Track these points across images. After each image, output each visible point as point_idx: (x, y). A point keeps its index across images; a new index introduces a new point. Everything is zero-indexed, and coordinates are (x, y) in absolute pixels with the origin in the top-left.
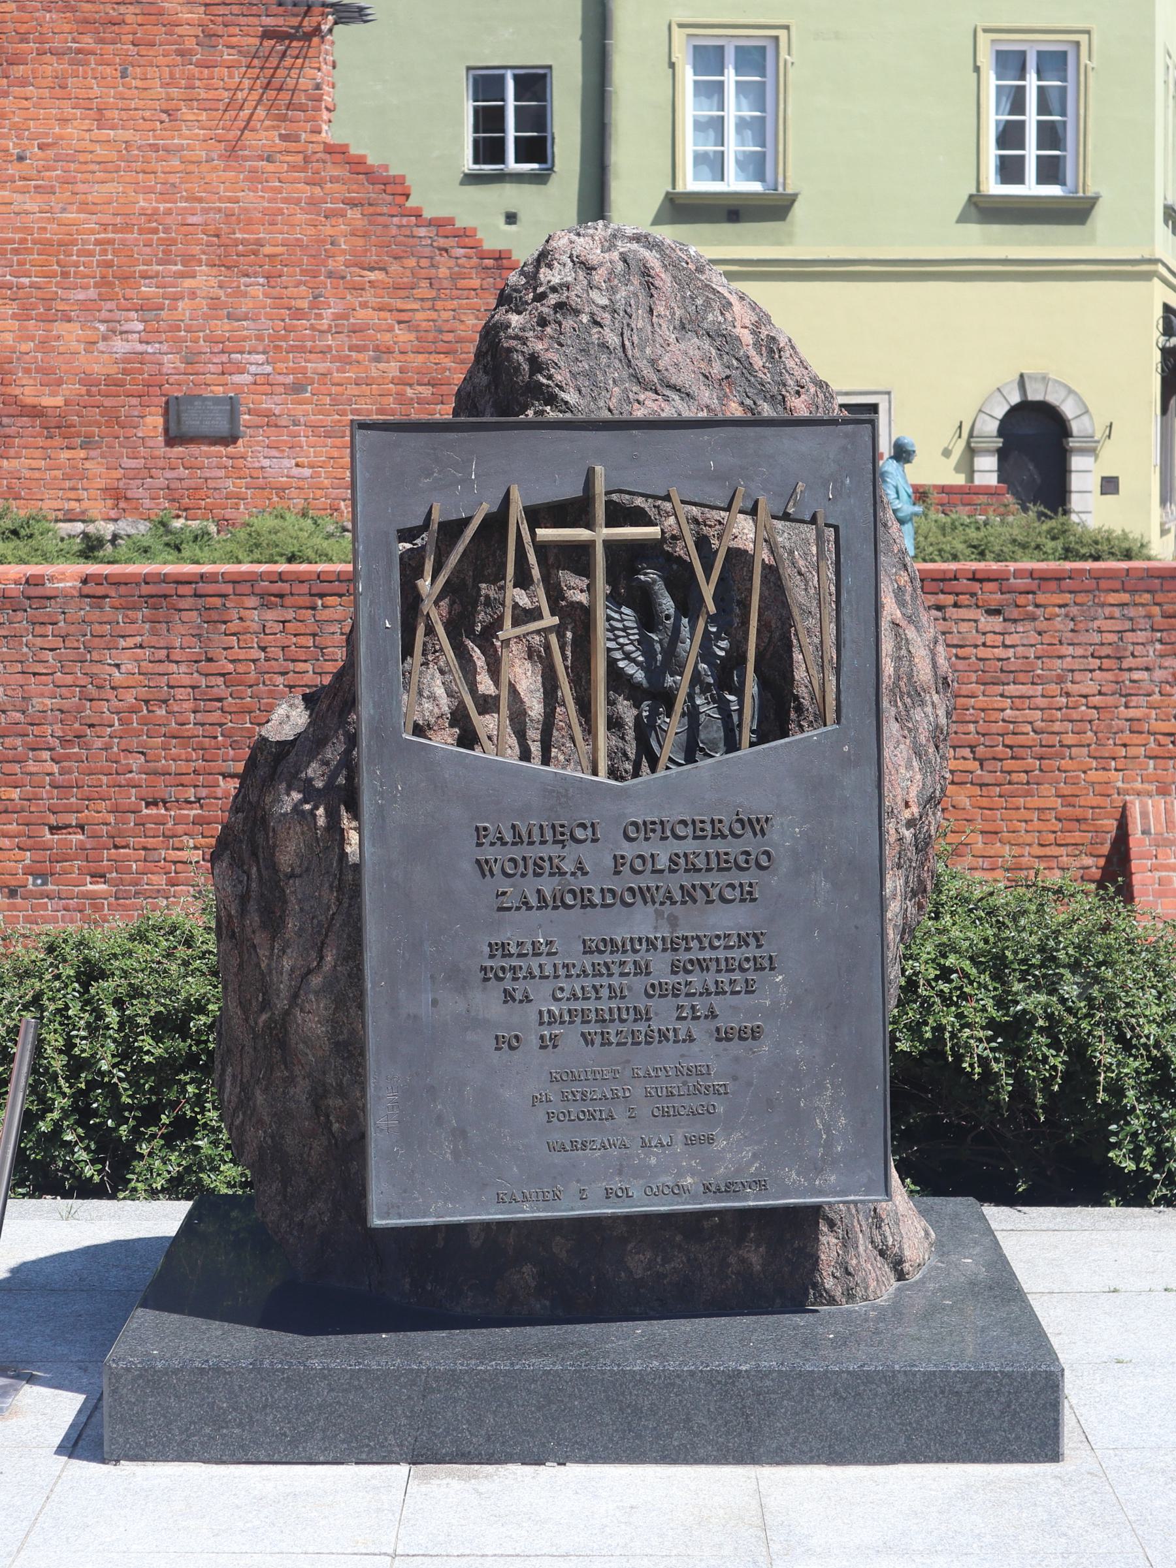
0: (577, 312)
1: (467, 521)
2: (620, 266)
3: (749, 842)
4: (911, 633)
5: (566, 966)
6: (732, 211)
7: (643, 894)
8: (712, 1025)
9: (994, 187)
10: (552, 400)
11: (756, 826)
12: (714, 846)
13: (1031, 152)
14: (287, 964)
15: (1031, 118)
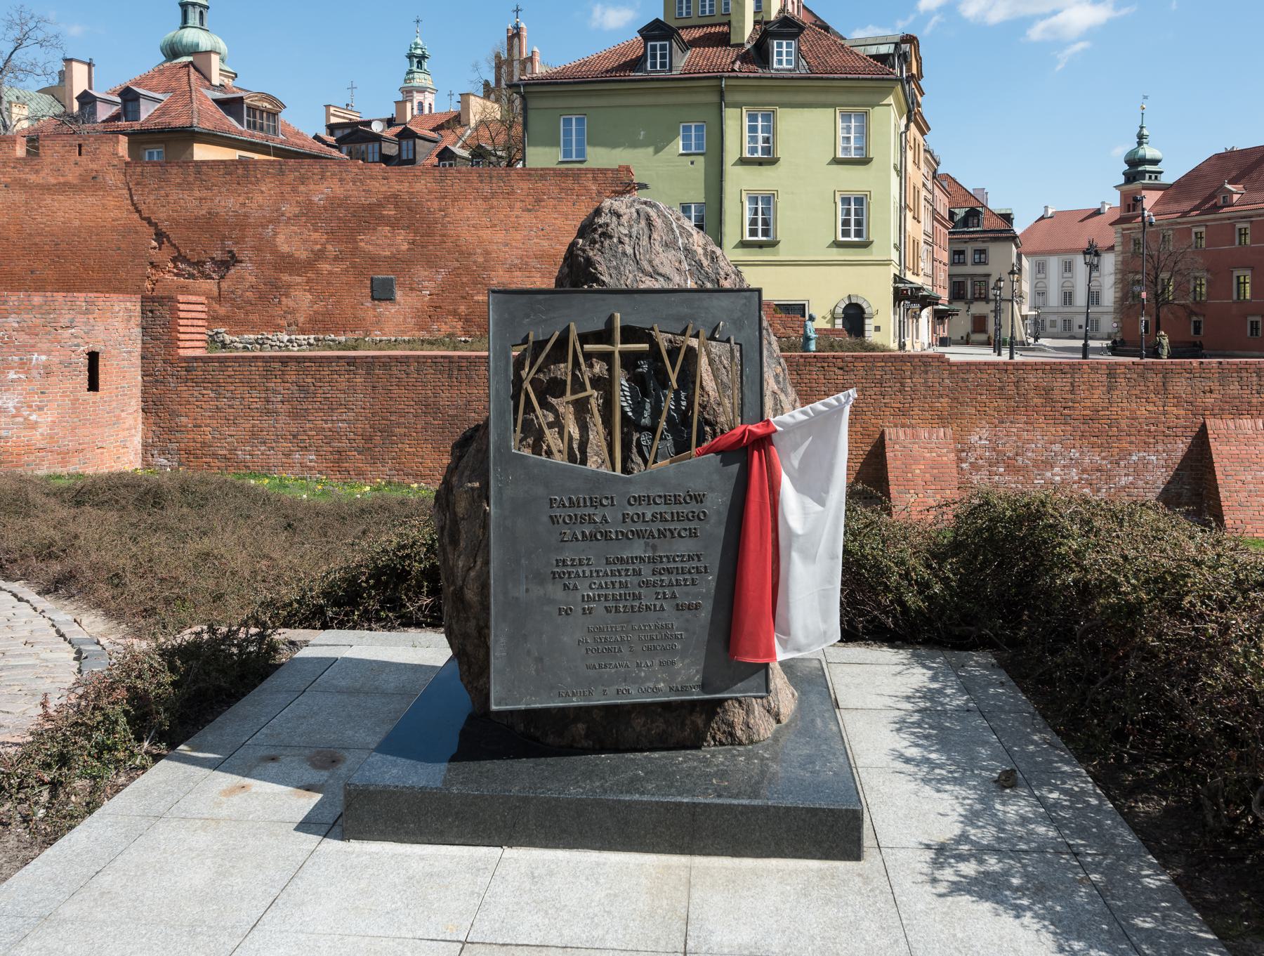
0: (611, 237)
1: (547, 341)
2: (635, 215)
3: (694, 507)
4: (782, 397)
5: (597, 572)
6: (760, 245)
7: (638, 534)
8: (674, 602)
9: (840, 238)
10: (597, 280)
11: (698, 499)
12: (676, 509)
13: (853, 228)
14: (461, 564)
15: (853, 217)
